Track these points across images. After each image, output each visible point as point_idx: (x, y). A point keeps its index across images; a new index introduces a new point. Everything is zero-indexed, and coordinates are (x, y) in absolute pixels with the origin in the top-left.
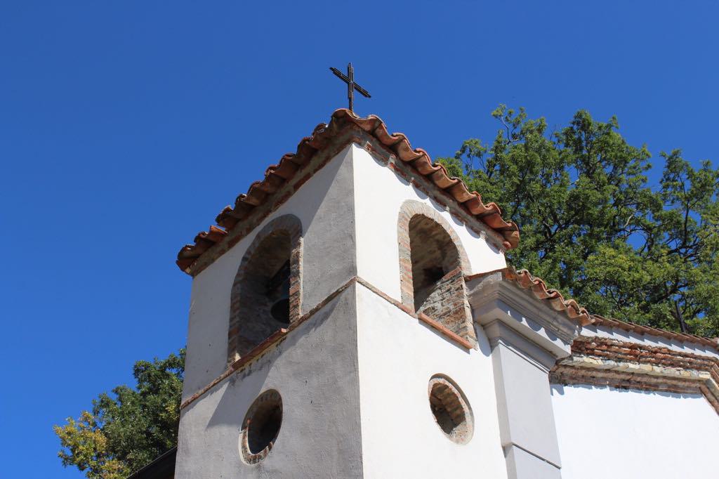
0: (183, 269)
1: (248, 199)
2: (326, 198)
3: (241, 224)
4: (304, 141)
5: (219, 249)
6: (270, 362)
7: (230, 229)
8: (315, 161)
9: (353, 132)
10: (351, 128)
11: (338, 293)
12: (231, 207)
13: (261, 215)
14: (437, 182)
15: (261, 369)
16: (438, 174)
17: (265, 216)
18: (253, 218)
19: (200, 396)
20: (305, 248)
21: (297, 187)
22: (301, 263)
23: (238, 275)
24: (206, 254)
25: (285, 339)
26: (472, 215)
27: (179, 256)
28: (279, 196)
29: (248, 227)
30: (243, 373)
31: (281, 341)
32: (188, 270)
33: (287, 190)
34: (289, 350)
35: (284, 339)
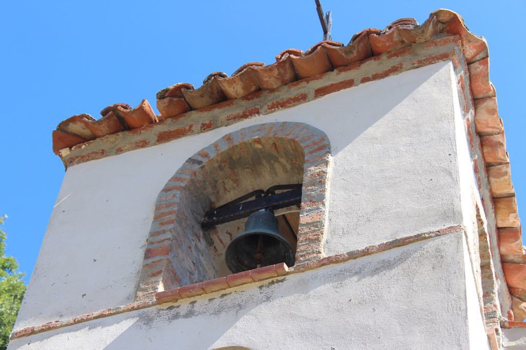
0: (57, 149)
1: (231, 82)
2: (388, 116)
3: (194, 115)
4: (369, 33)
5: (137, 138)
6: (240, 308)
7: (169, 115)
8: (370, 66)
9: (456, 48)
10: (455, 41)
11: (419, 238)
12: (197, 84)
13: (240, 111)
14: (492, 180)
15: (217, 312)
16: (500, 169)
17: (245, 116)
18: (220, 113)
19: (62, 326)
20: (335, 170)
21: (321, 92)
22: (328, 186)
23: (175, 178)
24: (112, 138)
25: (282, 281)
26: (499, 249)
27: (60, 126)
28: (424, 52)
29: (207, 122)
30: (173, 312)
31: (273, 283)
32: (65, 152)
33: (302, 91)
34: (291, 298)
35: (278, 281)
